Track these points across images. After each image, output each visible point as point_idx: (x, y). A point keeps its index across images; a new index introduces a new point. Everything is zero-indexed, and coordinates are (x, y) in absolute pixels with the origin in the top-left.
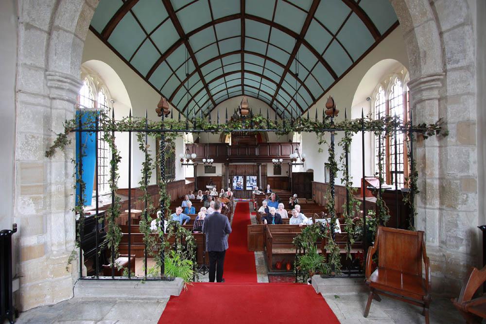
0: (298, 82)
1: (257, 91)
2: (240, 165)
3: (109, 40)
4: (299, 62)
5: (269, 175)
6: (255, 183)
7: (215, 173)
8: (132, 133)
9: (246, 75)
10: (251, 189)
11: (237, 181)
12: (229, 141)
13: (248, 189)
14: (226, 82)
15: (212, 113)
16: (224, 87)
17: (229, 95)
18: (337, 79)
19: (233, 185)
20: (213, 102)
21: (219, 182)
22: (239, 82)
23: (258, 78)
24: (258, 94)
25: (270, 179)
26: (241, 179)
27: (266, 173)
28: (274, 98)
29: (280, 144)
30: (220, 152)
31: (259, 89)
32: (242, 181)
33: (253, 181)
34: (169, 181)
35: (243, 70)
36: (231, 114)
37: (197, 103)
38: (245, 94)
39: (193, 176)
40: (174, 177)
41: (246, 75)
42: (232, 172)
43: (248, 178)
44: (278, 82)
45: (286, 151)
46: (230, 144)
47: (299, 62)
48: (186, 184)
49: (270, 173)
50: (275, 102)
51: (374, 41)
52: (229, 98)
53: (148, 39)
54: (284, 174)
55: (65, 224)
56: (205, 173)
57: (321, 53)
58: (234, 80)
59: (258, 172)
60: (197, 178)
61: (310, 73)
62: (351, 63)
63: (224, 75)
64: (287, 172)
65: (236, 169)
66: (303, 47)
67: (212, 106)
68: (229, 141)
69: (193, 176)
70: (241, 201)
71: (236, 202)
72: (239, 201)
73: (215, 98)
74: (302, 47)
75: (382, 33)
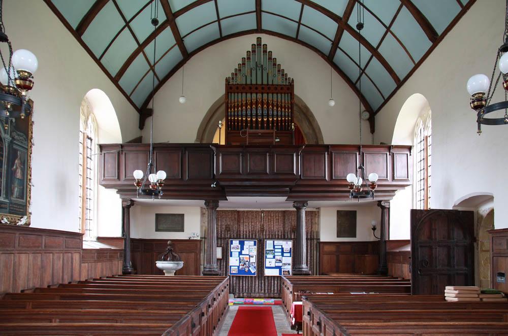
0: (362, 47)
3: (83, 37)
4: (364, 7)
5: (324, 238)
6: (288, 260)
7: (182, 230)
10: (275, 273)
11: (240, 253)
13: (268, 273)
19: (231, 264)
20: (180, 40)
26: (250, 248)
27: (318, 233)
29: (358, 148)
30: (194, 171)
32: (254, 252)
33: (283, 252)
39: (118, 233)
42: (228, 229)
43: (269, 244)
47: (364, 7)
49: (328, 233)
50: (348, 40)
51: (431, 44)
52: (222, 39)
54: (363, 234)
56: (157, 230)
57: (375, 45)
59: (297, 230)
62: (413, 65)
64: (374, 229)
65: (239, 221)
67: (176, 53)
68: (220, 138)
70: (252, 303)
71: (237, 307)
72: (245, 303)
75: (440, 33)
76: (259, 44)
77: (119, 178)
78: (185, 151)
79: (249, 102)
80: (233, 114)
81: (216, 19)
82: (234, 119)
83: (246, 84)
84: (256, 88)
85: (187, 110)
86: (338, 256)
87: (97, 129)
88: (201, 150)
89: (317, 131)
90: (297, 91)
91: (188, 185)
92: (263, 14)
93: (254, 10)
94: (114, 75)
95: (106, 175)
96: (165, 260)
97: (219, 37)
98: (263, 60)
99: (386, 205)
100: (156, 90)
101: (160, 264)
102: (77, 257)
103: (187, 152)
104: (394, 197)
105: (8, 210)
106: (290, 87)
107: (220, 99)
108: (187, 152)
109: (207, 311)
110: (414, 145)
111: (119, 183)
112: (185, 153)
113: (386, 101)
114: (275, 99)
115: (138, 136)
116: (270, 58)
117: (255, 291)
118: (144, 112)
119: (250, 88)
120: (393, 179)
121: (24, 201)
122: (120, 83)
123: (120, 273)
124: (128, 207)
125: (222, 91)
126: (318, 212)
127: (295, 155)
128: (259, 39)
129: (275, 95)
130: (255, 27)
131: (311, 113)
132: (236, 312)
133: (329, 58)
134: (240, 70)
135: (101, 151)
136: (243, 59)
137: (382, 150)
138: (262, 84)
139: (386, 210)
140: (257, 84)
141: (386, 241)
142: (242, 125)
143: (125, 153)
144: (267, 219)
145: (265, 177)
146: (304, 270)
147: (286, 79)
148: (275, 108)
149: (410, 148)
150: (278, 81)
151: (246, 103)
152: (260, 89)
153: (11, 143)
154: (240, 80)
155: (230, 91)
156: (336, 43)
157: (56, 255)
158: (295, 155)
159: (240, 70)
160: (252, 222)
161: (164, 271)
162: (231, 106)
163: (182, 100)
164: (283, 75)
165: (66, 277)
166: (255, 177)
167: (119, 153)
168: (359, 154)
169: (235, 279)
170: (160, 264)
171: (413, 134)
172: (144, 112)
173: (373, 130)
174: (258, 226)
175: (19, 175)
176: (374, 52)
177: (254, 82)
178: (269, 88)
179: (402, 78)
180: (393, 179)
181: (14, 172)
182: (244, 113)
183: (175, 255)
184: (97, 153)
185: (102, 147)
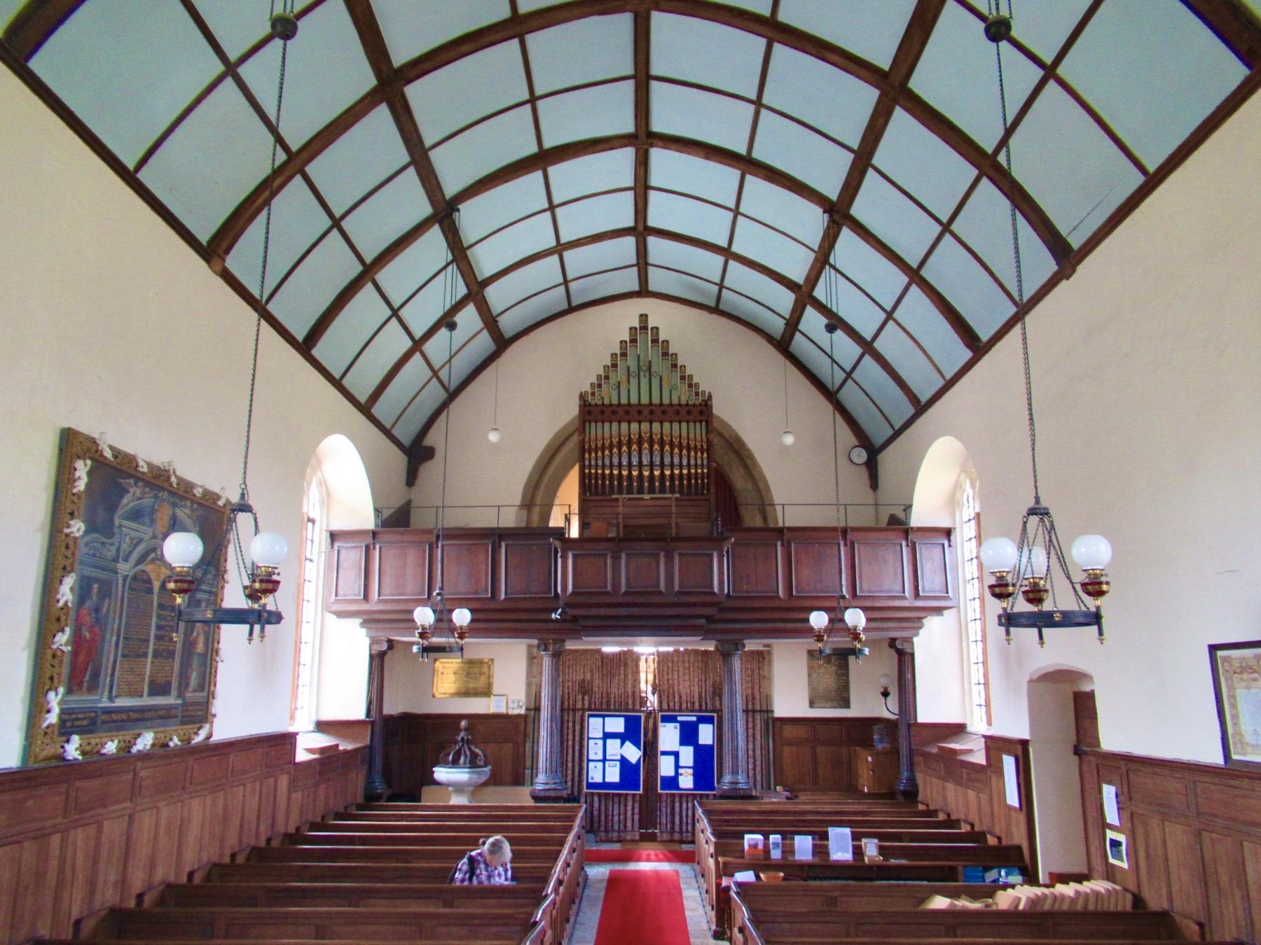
1: (710, 264)
9: (663, 163)
14: (552, 208)
16: (539, 235)
17: (572, 286)
18: (1067, 258)
20: (490, 321)
21: (509, 747)
22: (622, 212)
23: (722, 179)
24: (721, 286)
25: (788, 732)
27: (768, 699)
28: (804, 294)
31: (727, 253)
34: (145, 741)
35: (641, 228)
37: (395, 313)
38: (652, 287)
39: (359, 713)
40: (200, 713)
41: (663, 163)
44: (798, 275)
45: (885, 575)
46: (574, 533)
48: (301, 756)
50: (812, 321)
52: (571, 309)
53: (335, 231)
58: (594, 191)
60: (390, 721)
61: (946, 228)
63: (544, 159)
64: (885, 694)
66: (846, 235)
67: (485, 342)
68: (565, 513)
69: (359, 713)
73: (496, 296)
74: (846, 235)
76: (644, 328)
77: (366, 597)
79: (625, 439)
80: (593, 462)
83: (619, 405)
84: (640, 412)
85: (502, 453)
86: (814, 749)
87: (327, 499)
88: (534, 538)
89: (761, 485)
90: (718, 409)
92: (651, 269)
93: (634, 262)
94: (363, 399)
95: (340, 592)
96: (455, 763)
97: (565, 306)
98: (652, 354)
99: (906, 647)
100: (444, 406)
102: (284, 781)
104: (921, 632)
105: (179, 719)
107: (572, 421)
108: (503, 544)
110: (958, 526)
111: (365, 607)
112: (500, 546)
113: (897, 433)
114: (676, 433)
116: (665, 354)
118: (417, 454)
119: (628, 412)
120: (917, 595)
121: (205, 694)
122: (376, 411)
123: (360, 800)
124: (382, 655)
125: (571, 411)
126: (769, 653)
127: (715, 555)
128: (644, 317)
129: (676, 425)
130: (636, 288)
131: (748, 450)
132: (605, 884)
133: (783, 345)
134: (607, 378)
136: (614, 355)
137: (891, 535)
138: (651, 404)
139: (907, 658)
140: (639, 404)
142: (611, 484)
145: (656, 599)
146: (740, 786)
147: (697, 394)
148: (676, 450)
149: (948, 533)
150: (681, 395)
152: (646, 412)
154: (609, 395)
155: (587, 417)
156: (793, 324)
157: (249, 787)
158: (715, 555)
159: (607, 378)
163: (493, 437)
164: (690, 386)
165: (263, 827)
167: (367, 547)
168: (845, 545)
169: (596, 799)
171: (953, 502)
172: (417, 454)
173: (874, 484)
175: (200, 647)
176: (868, 347)
177: (634, 400)
178: (664, 412)
179: (924, 398)
180: (917, 595)
181: (194, 643)
182: (615, 461)
183: (478, 751)
184: (323, 549)
185: (334, 536)
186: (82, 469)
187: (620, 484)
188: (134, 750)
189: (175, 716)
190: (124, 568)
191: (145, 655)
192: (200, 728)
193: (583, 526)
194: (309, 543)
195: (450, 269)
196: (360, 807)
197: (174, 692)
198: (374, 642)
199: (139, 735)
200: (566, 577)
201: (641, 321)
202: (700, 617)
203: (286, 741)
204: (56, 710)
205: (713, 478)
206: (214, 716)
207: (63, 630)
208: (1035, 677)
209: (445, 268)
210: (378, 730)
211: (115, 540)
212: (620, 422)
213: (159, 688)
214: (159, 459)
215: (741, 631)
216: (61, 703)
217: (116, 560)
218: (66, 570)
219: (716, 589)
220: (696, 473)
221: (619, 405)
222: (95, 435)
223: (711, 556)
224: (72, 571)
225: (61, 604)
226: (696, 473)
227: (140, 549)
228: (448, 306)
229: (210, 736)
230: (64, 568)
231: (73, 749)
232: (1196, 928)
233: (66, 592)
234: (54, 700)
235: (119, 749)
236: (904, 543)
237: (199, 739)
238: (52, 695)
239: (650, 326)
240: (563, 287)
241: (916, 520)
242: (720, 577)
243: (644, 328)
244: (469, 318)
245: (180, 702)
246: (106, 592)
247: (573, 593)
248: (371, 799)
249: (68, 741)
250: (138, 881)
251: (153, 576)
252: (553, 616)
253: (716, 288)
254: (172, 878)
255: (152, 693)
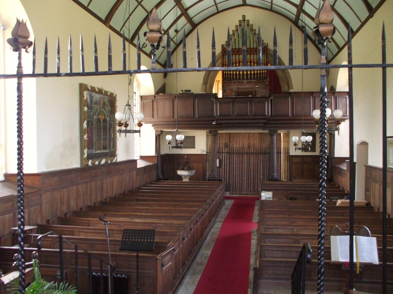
2: (239, 133)
7: (194, 147)
8: (82, 72)
12: (218, 90)
15: (188, 40)
17: (218, 5)
20: (190, 20)
21: (201, 165)
25: (294, 160)
34: (103, 162)
36: (221, 40)
39: (152, 153)
40: (113, 154)
46: (220, 96)
48: (139, 166)
50: (303, 17)
52: (218, 12)
55: (277, 250)
62: (360, 24)
67: (188, 27)
68: (218, 90)
69: (152, 153)
76: (244, 20)
78: (195, 98)
79: (237, 61)
81: (214, 4)
82: (228, 73)
83: (235, 49)
91: (198, 121)
96: (183, 169)
97: (216, 11)
101: (180, 172)
102: (135, 173)
103: (197, 99)
106: (265, 49)
108: (197, 99)
109: (212, 203)
115: (167, 91)
117: (244, 189)
121: (114, 149)
123: (155, 179)
124: (159, 135)
135: (141, 101)
139: (332, 136)
141: (332, 158)
143: (157, 101)
144: (252, 139)
145: (246, 117)
146: (275, 177)
151: (236, 62)
153: (110, 121)
156: (298, 16)
160: (242, 141)
161: (183, 177)
162: (225, 64)
165: (130, 186)
166: (240, 117)
167: (153, 101)
170: (180, 172)
174: (246, 145)
186: (85, 93)
187: (236, 77)
188: (101, 163)
189: (108, 155)
190: (95, 117)
191: (101, 140)
192: (114, 158)
193: (224, 92)
194: (134, 100)
195: (175, 8)
196: (155, 182)
197: (108, 149)
198: (156, 131)
199: (102, 160)
200: (217, 110)
201: (243, 18)
202: (261, 123)
203: (134, 162)
204: (86, 154)
205: (268, 74)
206: (117, 155)
207: (85, 135)
208: (359, 144)
209: (174, 7)
210: (159, 158)
211: (93, 110)
212: (236, 55)
213: (105, 148)
214: (100, 87)
215: (277, 127)
216: (87, 152)
217: (93, 116)
218: (85, 120)
219: (266, 114)
220: (262, 72)
221: (235, 49)
222: (86, 83)
223: (265, 103)
224: (85, 120)
225: (84, 128)
226: (262, 72)
227: (98, 111)
228: (175, 19)
229: (116, 160)
230: (84, 119)
231: (90, 163)
232: (377, 209)
233: (85, 125)
234: (86, 151)
235: (98, 163)
236: (333, 97)
237: (114, 161)
238: (85, 150)
239: (246, 19)
240: (215, 6)
241: (338, 90)
242: (268, 110)
243: (244, 20)
244: (183, 20)
245: (109, 151)
246: (92, 124)
247: (219, 116)
248: (158, 179)
249: (89, 161)
250: (105, 196)
251: (101, 118)
252: (213, 123)
253: (270, 4)
254: (111, 196)
255: (104, 149)
